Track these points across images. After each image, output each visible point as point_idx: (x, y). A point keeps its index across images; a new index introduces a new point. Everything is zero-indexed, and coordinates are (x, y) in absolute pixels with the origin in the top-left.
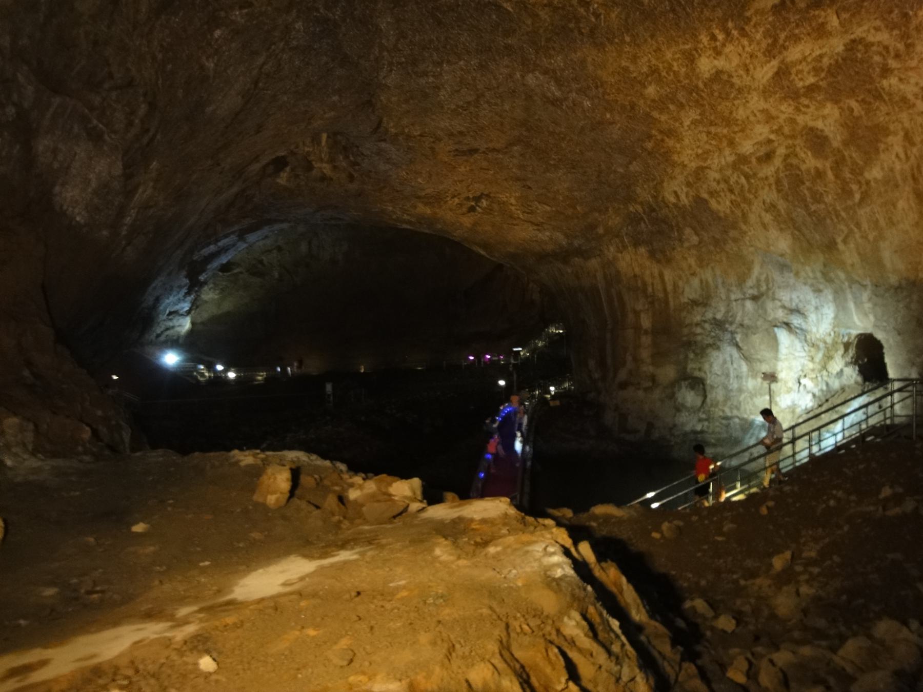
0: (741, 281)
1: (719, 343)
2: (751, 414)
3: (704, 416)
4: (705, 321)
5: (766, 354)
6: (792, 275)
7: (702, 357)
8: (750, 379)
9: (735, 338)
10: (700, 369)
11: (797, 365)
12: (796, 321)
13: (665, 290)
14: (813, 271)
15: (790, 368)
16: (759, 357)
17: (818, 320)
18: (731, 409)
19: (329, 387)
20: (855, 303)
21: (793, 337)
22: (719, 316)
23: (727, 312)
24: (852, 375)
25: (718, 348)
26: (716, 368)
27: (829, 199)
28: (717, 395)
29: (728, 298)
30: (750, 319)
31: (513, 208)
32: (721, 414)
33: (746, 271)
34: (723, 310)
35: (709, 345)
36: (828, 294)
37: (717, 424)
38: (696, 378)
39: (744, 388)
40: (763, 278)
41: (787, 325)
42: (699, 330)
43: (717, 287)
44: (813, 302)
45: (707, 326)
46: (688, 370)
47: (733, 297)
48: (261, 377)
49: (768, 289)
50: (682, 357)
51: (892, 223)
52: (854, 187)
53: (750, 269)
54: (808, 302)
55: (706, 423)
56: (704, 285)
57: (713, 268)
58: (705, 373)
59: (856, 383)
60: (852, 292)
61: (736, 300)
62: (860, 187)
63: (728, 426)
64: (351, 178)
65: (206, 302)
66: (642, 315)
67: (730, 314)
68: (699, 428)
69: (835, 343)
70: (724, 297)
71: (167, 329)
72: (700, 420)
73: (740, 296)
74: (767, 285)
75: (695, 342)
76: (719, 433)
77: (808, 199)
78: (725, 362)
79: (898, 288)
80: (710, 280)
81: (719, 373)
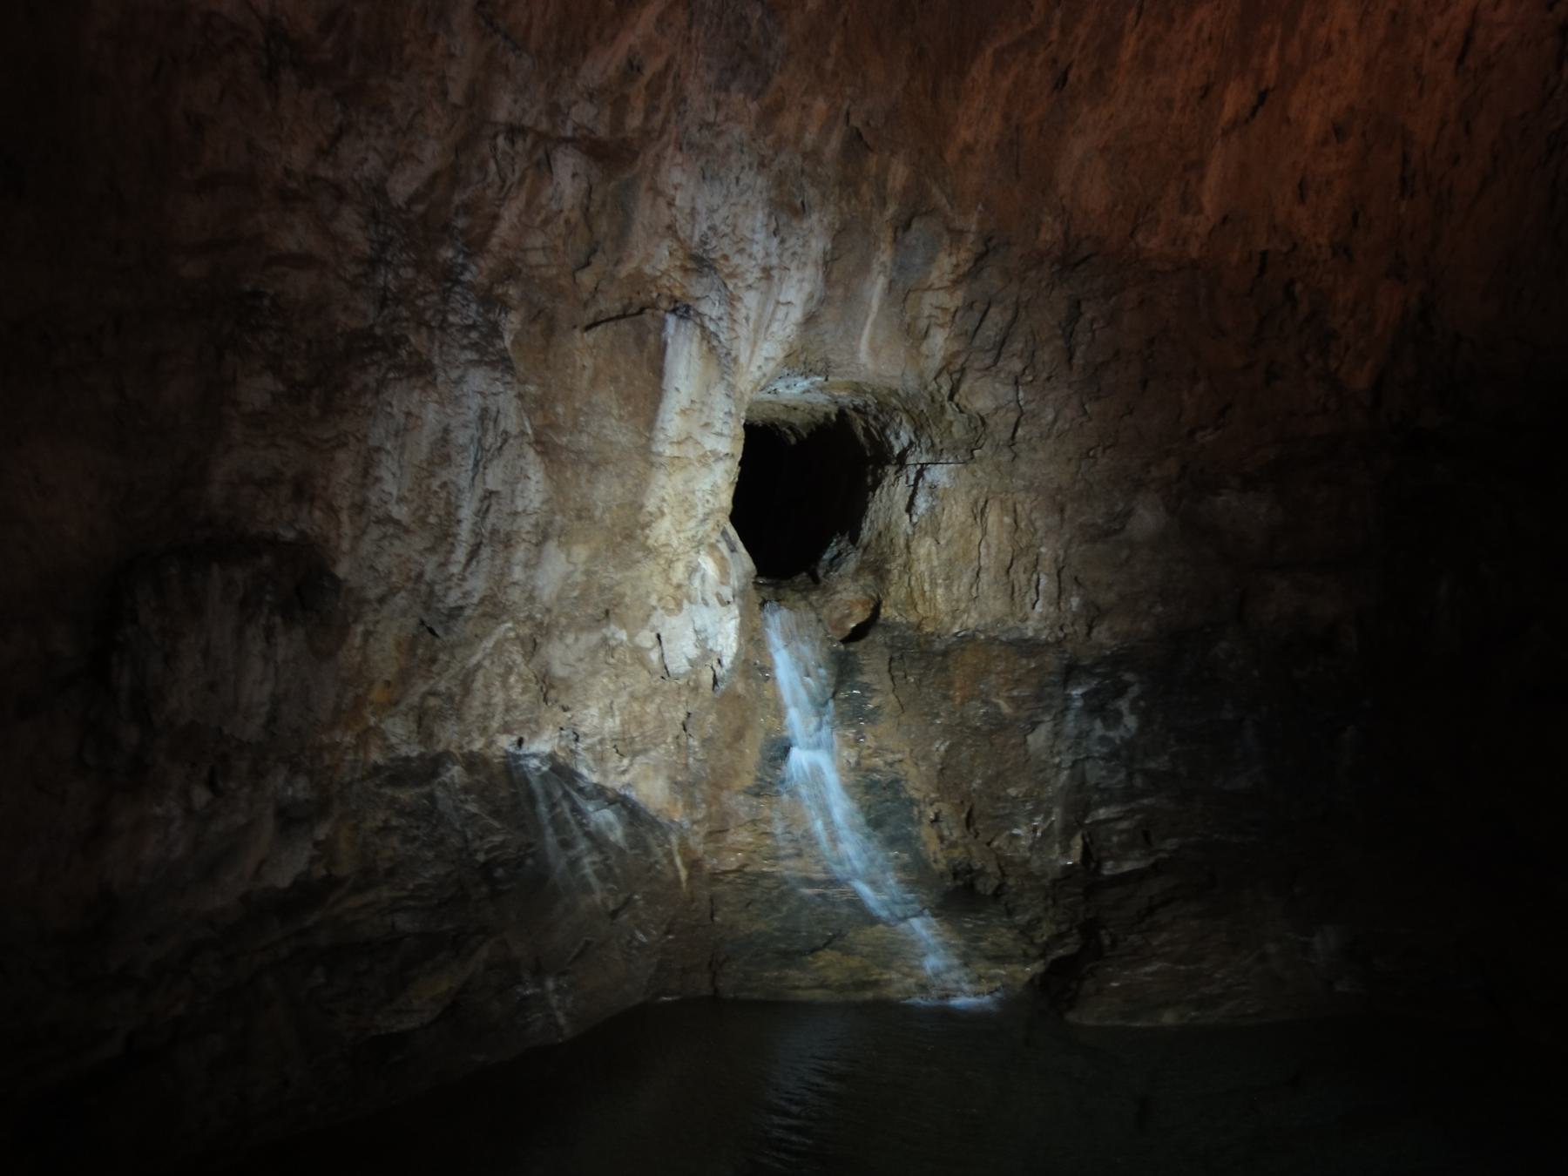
1: (418, 340)
8: (551, 547)
9: (495, 331)
10: (303, 490)
12: (711, 309)
18: (424, 720)
23: (452, 176)
25: (421, 371)
26: (391, 482)
29: (478, 96)
34: (432, 155)
40: (653, 66)
42: (296, 236)
58: (332, 510)
63: (428, 812)
70: (456, 95)
72: (290, 819)
78: (442, 452)
81: (400, 512)
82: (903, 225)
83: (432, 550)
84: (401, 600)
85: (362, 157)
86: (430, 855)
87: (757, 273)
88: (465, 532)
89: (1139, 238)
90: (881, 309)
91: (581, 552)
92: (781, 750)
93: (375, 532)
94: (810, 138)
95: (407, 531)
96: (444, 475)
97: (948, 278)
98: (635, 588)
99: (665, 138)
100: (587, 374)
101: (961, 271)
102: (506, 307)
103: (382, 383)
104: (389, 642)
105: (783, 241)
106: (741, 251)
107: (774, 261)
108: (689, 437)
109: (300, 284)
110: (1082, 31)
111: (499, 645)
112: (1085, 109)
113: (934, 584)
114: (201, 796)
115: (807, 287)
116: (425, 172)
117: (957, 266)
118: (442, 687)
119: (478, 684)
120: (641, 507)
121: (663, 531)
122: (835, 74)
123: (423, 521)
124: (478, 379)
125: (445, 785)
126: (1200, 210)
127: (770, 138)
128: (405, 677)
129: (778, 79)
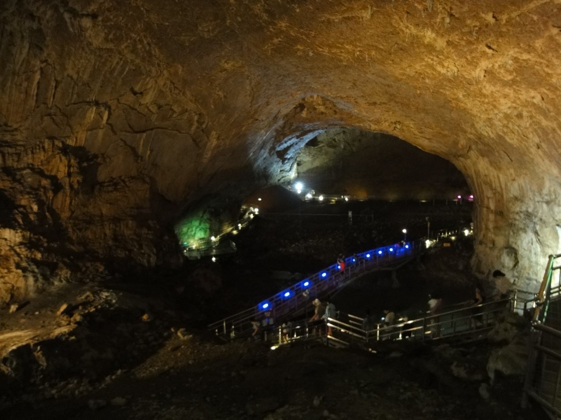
3: (516, 274)
7: (517, 236)
10: (516, 243)
13: (501, 187)
19: (350, 214)
22: (530, 210)
25: (525, 232)
26: (525, 245)
28: (524, 262)
30: (546, 216)
31: (413, 129)
32: (527, 275)
35: (521, 229)
37: (523, 281)
38: (513, 248)
42: (517, 217)
43: (527, 191)
48: (333, 201)
50: (507, 233)
56: (521, 188)
57: (524, 178)
58: (518, 246)
64: (335, 112)
65: (306, 162)
66: (490, 200)
71: (283, 177)
75: (515, 225)
76: (522, 287)
80: (523, 185)
81: (526, 248)
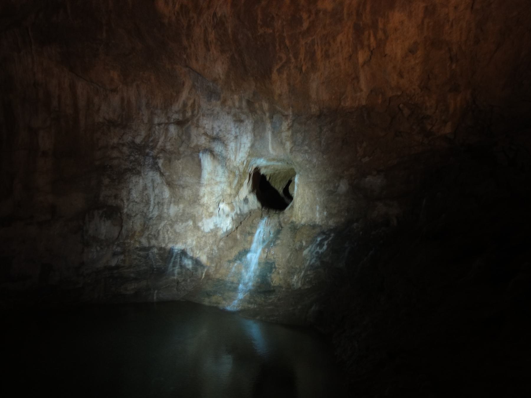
0: (167, 106)
1: (139, 168)
2: (169, 242)
3: (119, 249)
4: (123, 145)
5: (190, 180)
6: (219, 103)
8: (172, 205)
9: (157, 163)
10: (116, 197)
11: (218, 189)
12: (218, 148)
14: (240, 100)
15: (212, 193)
16: (182, 183)
17: (236, 148)
18: (148, 239)
20: (273, 132)
21: (216, 163)
22: (138, 140)
23: (148, 136)
24: (254, 203)
25: (139, 173)
26: (135, 195)
27: (278, 24)
29: (151, 121)
32: (137, 245)
33: (175, 94)
34: (143, 133)
36: (249, 125)
39: (165, 215)
40: (190, 102)
41: (211, 152)
42: (115, 154)
43: (140, 109)
44: (233, 133)
45: (125, 149)
46: (101, 198)
47: (156, 120)
49: (193, 116)
51: (327, 56)
52: (305, 16)
53: (179, 93)
54: (229, 132)
55: (122, 257)
58: (122, 200)
59: (258, 208)
60: (271, 122)
61: (159, 124)
62: (309, 17)
67: (151, 139)
68: (114, 263)
69: (244, 172)
70: (146, 121)
72: (115, 254)
73: (164, 120)
74: (193, 112)
77: (259, 22)
78: (145, 188)
79: (320, 116)
80: (133, 99)
81: (137, 200)
82: (271, 117)
83: (145, 207)
84: (139, 216)
85: (128, 138)
86: (144, 265)
87: (233, 138)
88: (152, 203)
89: (342, 104)
90: (272, 139)
91: (181, 206)
92: (246, 252)
93: (131, 204)
94: (237, 104)
95: (138, 203)
96: (146, 192)
97: (287, 127)
98: (198, 213)
99: (199, 115)
100: (181, 169)
101: (290, 125)
102: (159, 158)
103: (130, 177)
104: (138, 224)
105: (239, 129)
106: (228, 134)
107: (238, 134)
108: (212, 178)
109: (116, 162)
110: (302, 56)
111: (165, 225)
112: (312, 74)
113: (299, 210)
114: (98, 248)
115: (250, 138)
116: (143, 137)
117: (288, 125)
118: (152, 233)
119: (161, 233)
120: (198, 195)
121: (205, 200)
122: (236, 90)
123: (142, 201)
124: (151, 174)
125: (152, 253)
126: (361, 90)
127: (227, 107)
128: (143, 231)
129: (222, 96)
